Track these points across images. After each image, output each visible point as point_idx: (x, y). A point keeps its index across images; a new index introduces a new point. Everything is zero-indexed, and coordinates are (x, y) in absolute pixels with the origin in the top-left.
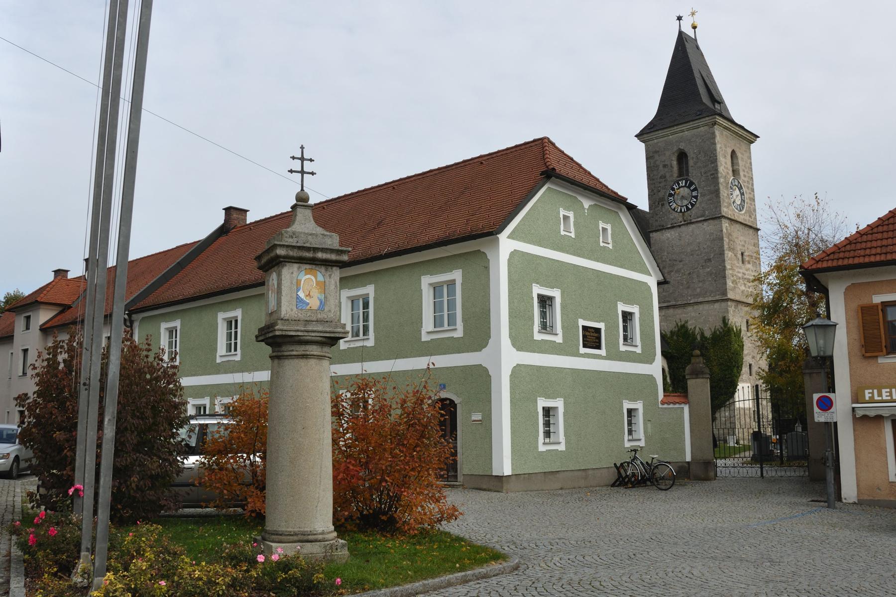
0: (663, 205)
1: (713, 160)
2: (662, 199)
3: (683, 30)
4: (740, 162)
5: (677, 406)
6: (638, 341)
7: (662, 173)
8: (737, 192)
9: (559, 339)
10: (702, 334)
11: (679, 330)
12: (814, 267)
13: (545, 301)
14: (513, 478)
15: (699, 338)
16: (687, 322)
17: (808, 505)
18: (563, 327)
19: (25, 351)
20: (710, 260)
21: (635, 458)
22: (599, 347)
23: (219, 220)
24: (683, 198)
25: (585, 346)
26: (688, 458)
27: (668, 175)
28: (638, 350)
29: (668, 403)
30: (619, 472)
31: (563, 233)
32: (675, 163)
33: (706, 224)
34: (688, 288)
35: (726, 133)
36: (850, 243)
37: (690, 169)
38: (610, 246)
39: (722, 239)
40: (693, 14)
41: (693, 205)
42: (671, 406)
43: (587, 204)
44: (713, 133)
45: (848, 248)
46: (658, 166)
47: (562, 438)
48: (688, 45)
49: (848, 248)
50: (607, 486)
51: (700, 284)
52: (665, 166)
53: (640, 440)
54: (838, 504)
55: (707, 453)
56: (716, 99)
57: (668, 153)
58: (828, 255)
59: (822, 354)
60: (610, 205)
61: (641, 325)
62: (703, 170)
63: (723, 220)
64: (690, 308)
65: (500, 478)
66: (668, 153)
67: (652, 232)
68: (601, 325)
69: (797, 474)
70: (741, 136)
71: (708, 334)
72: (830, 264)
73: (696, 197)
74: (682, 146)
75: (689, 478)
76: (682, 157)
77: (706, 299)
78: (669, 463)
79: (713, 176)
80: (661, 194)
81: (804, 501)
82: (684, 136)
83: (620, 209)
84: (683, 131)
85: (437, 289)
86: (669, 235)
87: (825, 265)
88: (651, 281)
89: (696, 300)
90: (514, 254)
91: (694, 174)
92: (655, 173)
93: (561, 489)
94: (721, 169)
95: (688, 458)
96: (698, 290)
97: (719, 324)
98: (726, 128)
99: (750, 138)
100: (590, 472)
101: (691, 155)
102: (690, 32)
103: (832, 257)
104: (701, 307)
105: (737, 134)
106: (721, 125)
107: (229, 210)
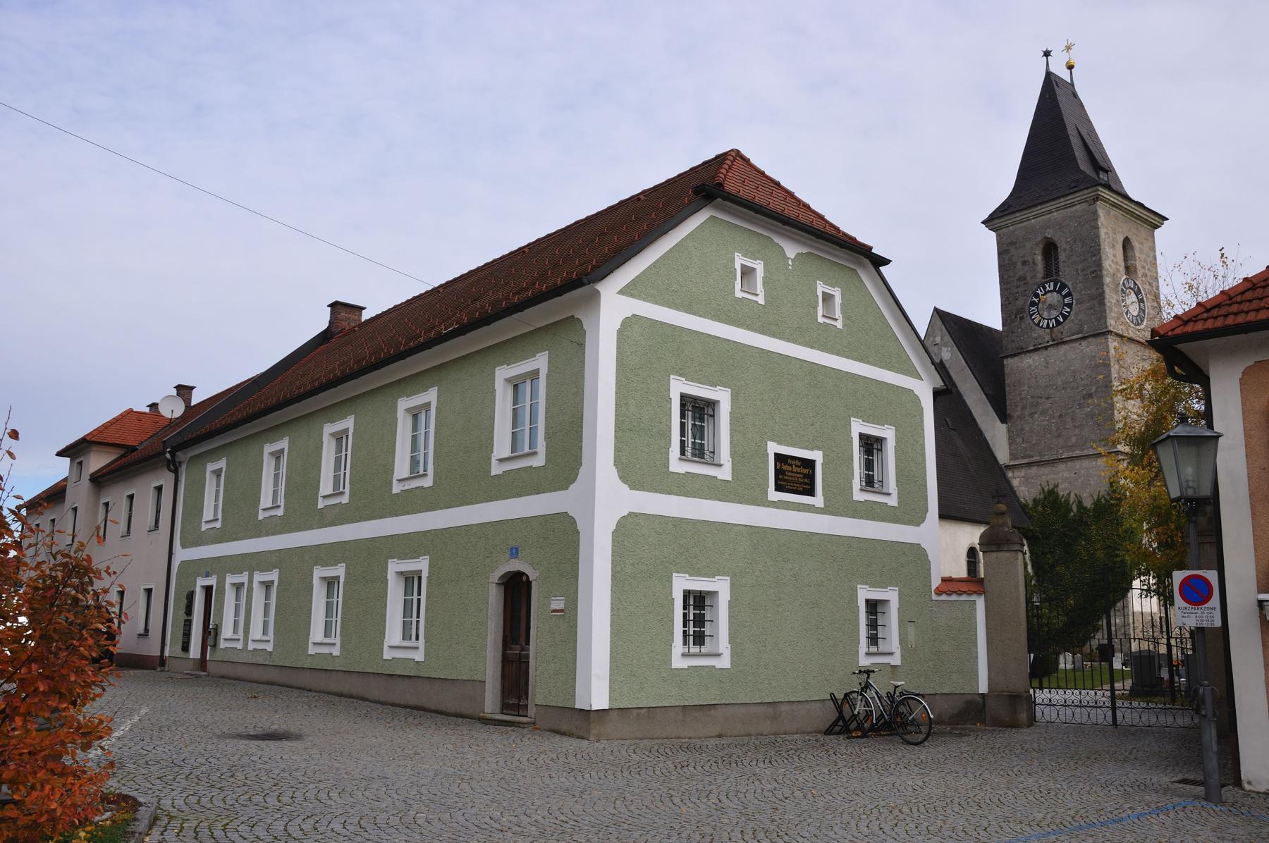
0: (1022, 318)
1: (1094, 251)
2: (1021, 310)
3: (1052, 69)
4: (1137, 254)
5: (964, 597)
6: (892, 484)
7: (1021, 273)
8: (1133, 297)
9: (725, 473)
10: (1080, 503)
11: (1045, 498)
12: (1178, 331)
13: (698, 410)
14: (614, 715)
15: (1074, 508)
16: (1056, 486)
17: (1166, 790)
18: (733, 454)
19: (75, 509)
20: (1090, 396)
21: (867, 686)
22: (810, 492)
23: (321, 322)
24: (1051, 307)
25: (779, 488)
26: (983, 688)
27: (1029, 276)
28: (892, 501)
29: (949, 593)
30: (839, 709)
31: (739, 294)
32: (1039, 258)
33: (1084, 343)
34: (1059, 436)
35: (1114, 212)
36: (1249, 285)
37: (1061, 265)
38: (839, 324)
39: (1107, 366)
40: (1068, 48)
41: (1065, 317)
42: (954, 597)
43: (791, 250)
44: (1095, 213)
45: (1249, 295)
46: (1014, 264)
47: (724, 645)
48: (1058, 91)
49: (1249, 295)
50: (819, 732)
51: (1077, 431)
52: (1024, 263)
53: (891, 654)
54: (1229, 793)
55: (1018, 676)
56: (1101, 166)
57: (1028, 245)
58: (1208, 311)
59: (1190, 493)
60: (841, 258)
61: (898, 459)
62: (1080, 267)
63: (1110, 338)
64: (1062, 466)
65: (586, 713)
66: (1028, 245)
67: (1007, 357)
68: (817, 456)
69: (1180, 721)
70: (1138, 217)
71: (1088, 503)
72: (1209, 324)
73: (1070, 306)
74: (1050, 233)
75: (983, 722)
76: (1050, 249)
77: (1086, 452)
78: (923, 696)
79: (1095, 274)
80: (1019, 303)
81: (1165, 780)
82: (1054, 218)
83: (862, 265)
84: (1050, 212)
85: (516, 385)
86: (1030, 361)
87: (1199, 326)
88: (923, 389)
89: (1070, 454)
90: (630, 325)
91: (1067, 273)
92: (1011, 273)
93: (720, 736)
94: (1107, 264)
95: (983, 688)
96: (1074, 440)
97: (1104, 488)
98: (1114, 205)
99: (1154, 220)
100: (784, 708)
101: (1062, 245)
102: (1064, 74)
103: (1214, 312)
104: (1077, 464)
105: (1132, 214)
106: (1106, 201)
107: (335, 306)
